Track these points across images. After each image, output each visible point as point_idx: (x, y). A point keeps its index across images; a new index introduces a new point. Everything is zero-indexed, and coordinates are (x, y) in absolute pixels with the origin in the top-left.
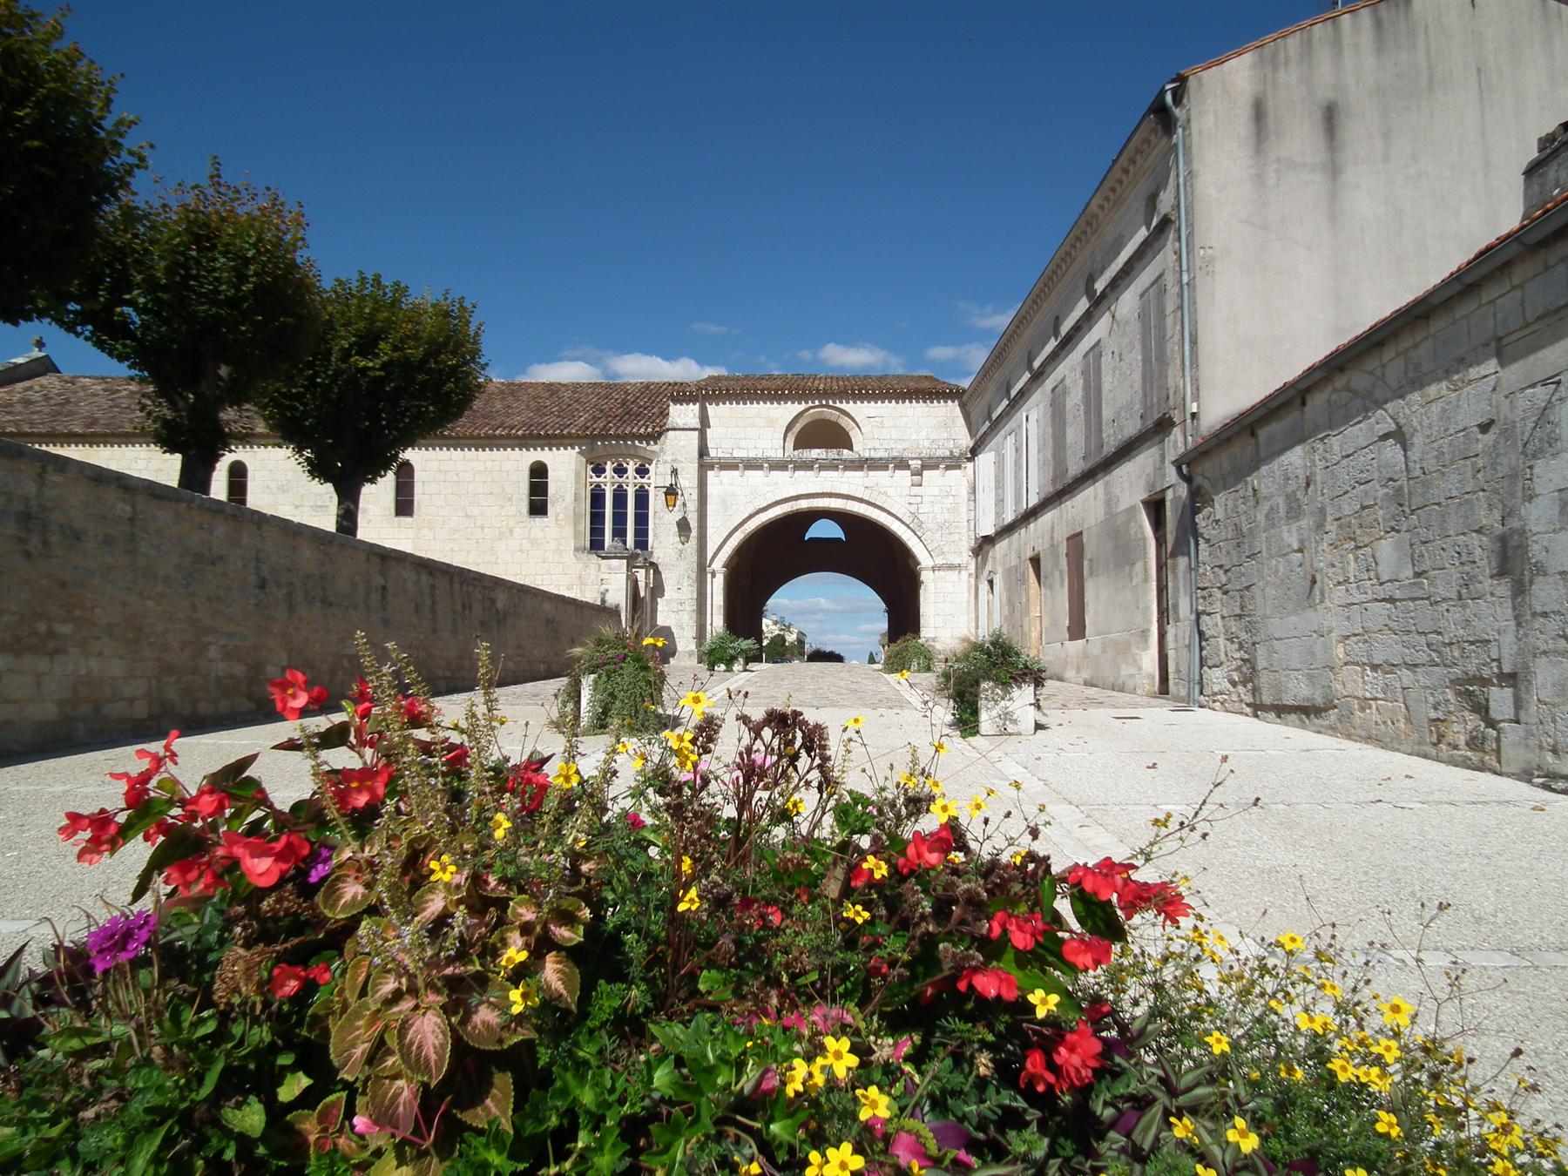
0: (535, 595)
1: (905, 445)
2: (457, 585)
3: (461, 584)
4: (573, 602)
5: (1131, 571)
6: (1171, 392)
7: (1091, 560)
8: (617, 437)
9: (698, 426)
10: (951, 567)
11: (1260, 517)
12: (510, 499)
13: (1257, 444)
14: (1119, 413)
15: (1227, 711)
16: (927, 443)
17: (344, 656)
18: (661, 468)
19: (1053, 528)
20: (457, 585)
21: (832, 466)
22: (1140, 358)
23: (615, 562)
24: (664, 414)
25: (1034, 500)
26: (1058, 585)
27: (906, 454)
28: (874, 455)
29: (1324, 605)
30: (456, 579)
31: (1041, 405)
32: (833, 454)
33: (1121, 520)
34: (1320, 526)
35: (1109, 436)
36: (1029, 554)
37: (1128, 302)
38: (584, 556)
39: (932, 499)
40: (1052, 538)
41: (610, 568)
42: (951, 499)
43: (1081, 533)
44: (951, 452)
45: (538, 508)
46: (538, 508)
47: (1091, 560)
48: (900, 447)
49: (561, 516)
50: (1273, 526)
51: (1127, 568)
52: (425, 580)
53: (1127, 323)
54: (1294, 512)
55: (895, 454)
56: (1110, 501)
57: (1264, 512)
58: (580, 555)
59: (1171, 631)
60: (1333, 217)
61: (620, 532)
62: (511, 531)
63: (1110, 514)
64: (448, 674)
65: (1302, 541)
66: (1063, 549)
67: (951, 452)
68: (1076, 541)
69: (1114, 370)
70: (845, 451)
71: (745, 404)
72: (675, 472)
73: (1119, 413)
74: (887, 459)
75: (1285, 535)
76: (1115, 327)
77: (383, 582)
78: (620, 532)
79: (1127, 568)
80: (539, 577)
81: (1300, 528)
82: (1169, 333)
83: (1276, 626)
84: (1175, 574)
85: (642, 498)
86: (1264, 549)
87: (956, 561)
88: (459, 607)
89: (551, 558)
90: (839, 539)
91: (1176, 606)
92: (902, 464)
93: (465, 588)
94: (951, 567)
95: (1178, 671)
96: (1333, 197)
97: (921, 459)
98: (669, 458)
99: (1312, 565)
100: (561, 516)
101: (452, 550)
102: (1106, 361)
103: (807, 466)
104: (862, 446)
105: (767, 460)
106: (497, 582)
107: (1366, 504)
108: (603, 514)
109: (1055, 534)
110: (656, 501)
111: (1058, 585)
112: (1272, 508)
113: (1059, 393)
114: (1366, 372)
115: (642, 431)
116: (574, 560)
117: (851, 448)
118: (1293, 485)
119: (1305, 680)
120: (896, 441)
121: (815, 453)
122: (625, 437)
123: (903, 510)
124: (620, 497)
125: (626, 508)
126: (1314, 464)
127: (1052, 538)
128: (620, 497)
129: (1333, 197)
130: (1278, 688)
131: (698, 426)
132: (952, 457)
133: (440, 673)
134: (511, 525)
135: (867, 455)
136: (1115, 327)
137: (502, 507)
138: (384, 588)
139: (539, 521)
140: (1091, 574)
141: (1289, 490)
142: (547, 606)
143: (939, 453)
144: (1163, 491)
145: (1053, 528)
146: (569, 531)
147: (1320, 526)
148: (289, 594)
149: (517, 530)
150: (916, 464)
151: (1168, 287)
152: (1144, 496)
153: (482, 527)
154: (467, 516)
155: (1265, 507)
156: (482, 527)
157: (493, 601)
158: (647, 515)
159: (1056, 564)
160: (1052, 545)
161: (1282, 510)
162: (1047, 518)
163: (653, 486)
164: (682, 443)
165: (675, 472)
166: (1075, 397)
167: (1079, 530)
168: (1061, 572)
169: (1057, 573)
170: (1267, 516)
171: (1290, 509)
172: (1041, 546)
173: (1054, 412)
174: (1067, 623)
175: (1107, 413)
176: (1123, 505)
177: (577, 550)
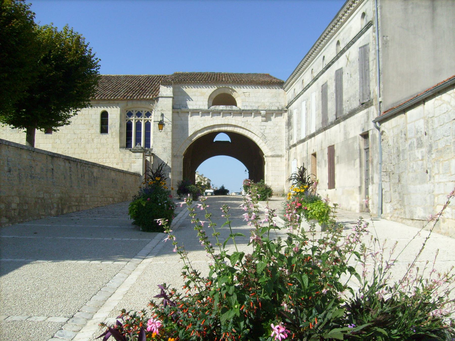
0: (108, 169)
1: (259, 105)
2: (79, 167)
3: (81, 166)
4: (122, 172)
5: (354, 162)
6: (372, 92)
7: (338, 157)
8: (137, 100)
9: (172, 96)
10: (278, 156)
11: (407, 145)
12: (92, 126)
13: (406, 117)
14: (350, 98)
15: (392, 220)
16: (268, 104)
17: (39, 198)
18: (156, 114)
19: (322, 142)
20: (79, 167)
21: (230, 113)
22: (359, 77)
23: (138, 154)
24: (157, 90)
25: (313, 131)
26: (323, 166)
27: (260, 109)
28: (246, 108)
29: (430, 182)
30: (79, 164)
31: (317, 92)
32: (228, 108)
33: (350, 141)
34: (430, 152)
35: (346, 107)
36: (312, 152)
37: (354, 51)
38: (124, 150)
39: (270, 127)
40: (322, 147)
41: (136, 156)
42: (277, 128)
43: (333, 146)
44: (278, 108)
45: (104, 129)
46: (104, 129)
47: (338, 157)
48: (257, 105)
49: (114, 134)
50: (412, 150)
51: (353, 161)
52: (67, 164)
53: (354, 62)
54: (420, 145)
55: (255, 108)
56: (346, 133)
57: (408, 144)
58: (122, 149)
59: (370, 187)
60: (433, 27)
61: (138, 140)
62: (93, 140)
63: (346, 139)
64: (77, 204)
65: (423, 157)
66: (326, 151)
67: (278, 108)
68: (331, 150)
69: (348, 80)
70: (234, 107)
71: (198, 88)
72: (162, 115)
73: (350, 98)
74: (252, 110)
75: (416, 153)
76: (349, 63)
77: (52, 167)
78: (138, 140)
79: (353, 161)
80: (105, 159)
81: (422, 152)
82: (371, 69)
83: (411, 188)
84: (372, 165)
85: (148, 126)
86: (408, 159)
87: (280, 153)
88: (80, 176)
89: (109, 152)
90: (228, 142)
91: (372, 178)
92: (257, 112)
93: (82, 167)
94: (278, 156)
95: (373, 204)
96: (433, 19)
97: (265, 110)
98: (160, 109)
99: (427, 166)
100: (114, 134)
101: (68, 148)
102: (345, 77)
103: (218, 113)
104: (240, 105)
105: (201, 110)
106: (94, 165)
107: (447, 144)
108: (141, 133)
109: (323, 145)
110: (154, 127)
111: (323, 166)
112: (411, 143)
113: (324, 88)
114: (448, 94)
115: (148, 97)
116: (119, 152)
117: (236, 105)
118: (419, 135)
119: (422, 210)
120: (255, 103)
121: (221, 107)
122: (140, 100)
123: (258, 132)
124: (138, 125)
125: (141, 130)
126: (428, 127)
127: (322, 147)
128: (138, 125)
129: (433, 19)
130: (411, 212)
131: (172, 96)
132: (279, 110)
133: (73, 203)
134: (93, 137)
135: (243, 109)
136: (349, 63)
137: (89, 130)
138: (53, 169)
139: (105, 136)
140: (338, 162)
141: (418, 136)
142: (113, 174)
143: (273, 108)
144: (368, 131)
145: (322, 142)
146: (117, 140)
147: (430, 152)
148: (19, 174)
149: (96, 140)
150: (263, 113)
151: (370, 50)
152: (361, 132)
153: (81, 138)
154: (74, 133)
155: (409, 142)
156: (81, 138)
157: (92, 173)
158: (150, 133)
159: (323, 157)
160: (322, 149)
161: (415, 144)
162: (320, 136)
163: (153, 121)
164: (165, 103)
165: (162, 115)
166: (331, 90)
167: (333, 144)
168: (325, 161)
169: (323, 161)
170: (410, 145)
171: (418, 144)
172: (317, 150)
173: (322, 95)
174: (327, 182)
175: (345, 97)
176: (352, 135)
177: (121, 147)
